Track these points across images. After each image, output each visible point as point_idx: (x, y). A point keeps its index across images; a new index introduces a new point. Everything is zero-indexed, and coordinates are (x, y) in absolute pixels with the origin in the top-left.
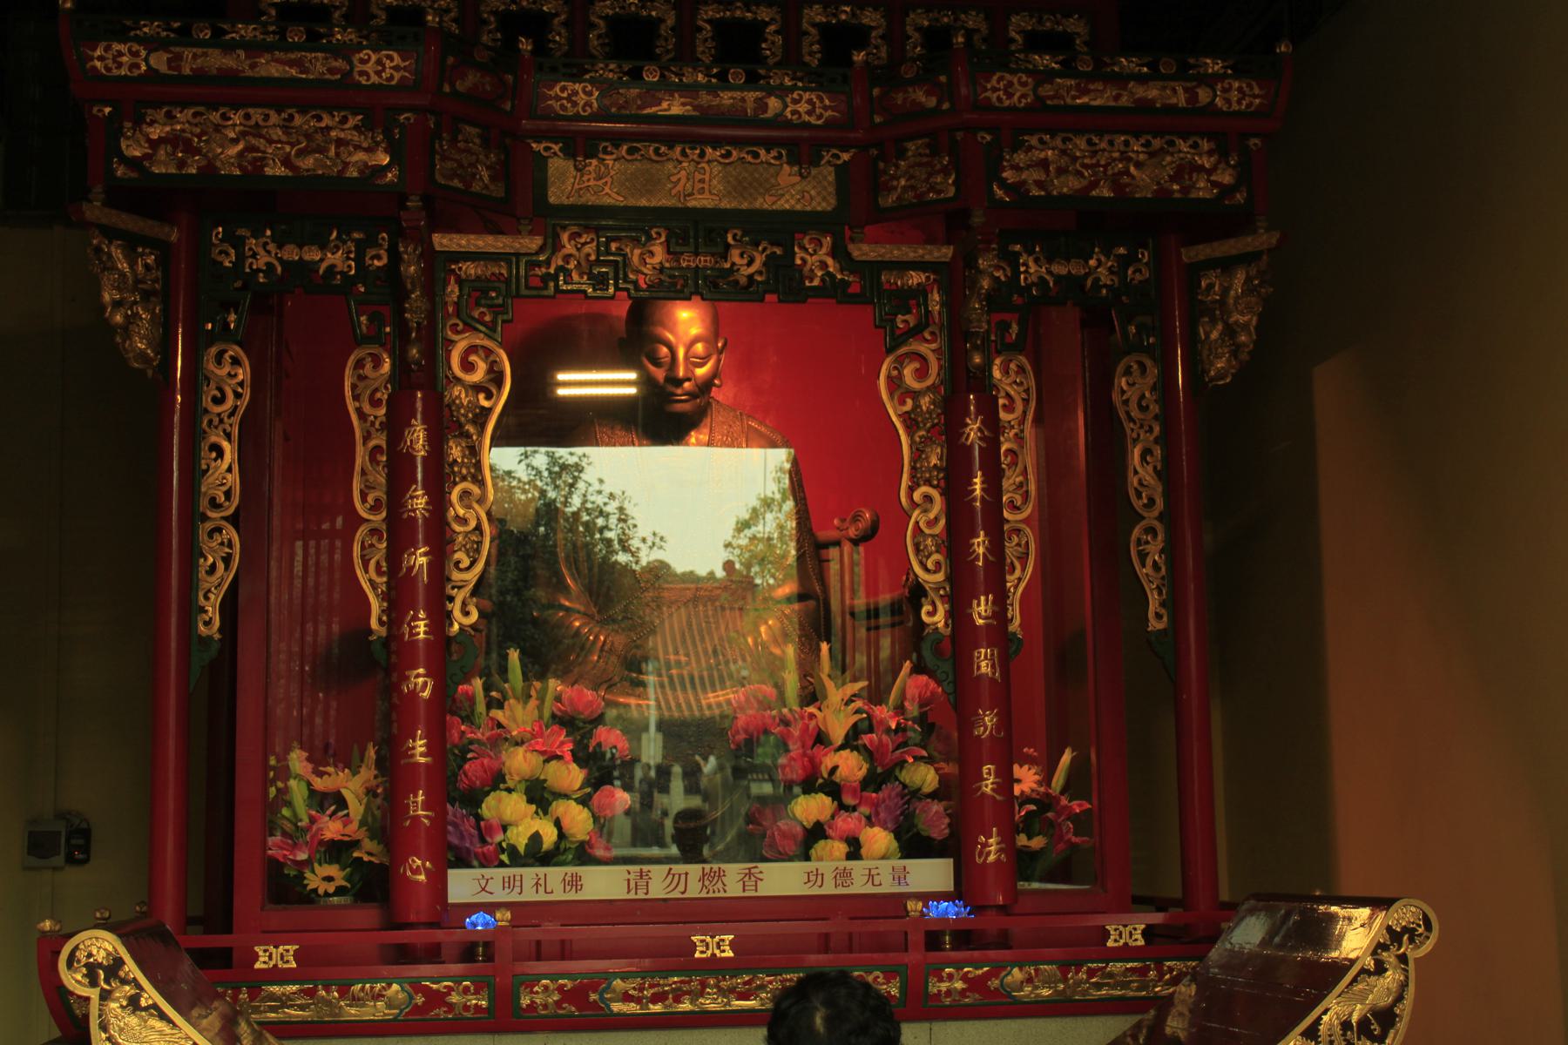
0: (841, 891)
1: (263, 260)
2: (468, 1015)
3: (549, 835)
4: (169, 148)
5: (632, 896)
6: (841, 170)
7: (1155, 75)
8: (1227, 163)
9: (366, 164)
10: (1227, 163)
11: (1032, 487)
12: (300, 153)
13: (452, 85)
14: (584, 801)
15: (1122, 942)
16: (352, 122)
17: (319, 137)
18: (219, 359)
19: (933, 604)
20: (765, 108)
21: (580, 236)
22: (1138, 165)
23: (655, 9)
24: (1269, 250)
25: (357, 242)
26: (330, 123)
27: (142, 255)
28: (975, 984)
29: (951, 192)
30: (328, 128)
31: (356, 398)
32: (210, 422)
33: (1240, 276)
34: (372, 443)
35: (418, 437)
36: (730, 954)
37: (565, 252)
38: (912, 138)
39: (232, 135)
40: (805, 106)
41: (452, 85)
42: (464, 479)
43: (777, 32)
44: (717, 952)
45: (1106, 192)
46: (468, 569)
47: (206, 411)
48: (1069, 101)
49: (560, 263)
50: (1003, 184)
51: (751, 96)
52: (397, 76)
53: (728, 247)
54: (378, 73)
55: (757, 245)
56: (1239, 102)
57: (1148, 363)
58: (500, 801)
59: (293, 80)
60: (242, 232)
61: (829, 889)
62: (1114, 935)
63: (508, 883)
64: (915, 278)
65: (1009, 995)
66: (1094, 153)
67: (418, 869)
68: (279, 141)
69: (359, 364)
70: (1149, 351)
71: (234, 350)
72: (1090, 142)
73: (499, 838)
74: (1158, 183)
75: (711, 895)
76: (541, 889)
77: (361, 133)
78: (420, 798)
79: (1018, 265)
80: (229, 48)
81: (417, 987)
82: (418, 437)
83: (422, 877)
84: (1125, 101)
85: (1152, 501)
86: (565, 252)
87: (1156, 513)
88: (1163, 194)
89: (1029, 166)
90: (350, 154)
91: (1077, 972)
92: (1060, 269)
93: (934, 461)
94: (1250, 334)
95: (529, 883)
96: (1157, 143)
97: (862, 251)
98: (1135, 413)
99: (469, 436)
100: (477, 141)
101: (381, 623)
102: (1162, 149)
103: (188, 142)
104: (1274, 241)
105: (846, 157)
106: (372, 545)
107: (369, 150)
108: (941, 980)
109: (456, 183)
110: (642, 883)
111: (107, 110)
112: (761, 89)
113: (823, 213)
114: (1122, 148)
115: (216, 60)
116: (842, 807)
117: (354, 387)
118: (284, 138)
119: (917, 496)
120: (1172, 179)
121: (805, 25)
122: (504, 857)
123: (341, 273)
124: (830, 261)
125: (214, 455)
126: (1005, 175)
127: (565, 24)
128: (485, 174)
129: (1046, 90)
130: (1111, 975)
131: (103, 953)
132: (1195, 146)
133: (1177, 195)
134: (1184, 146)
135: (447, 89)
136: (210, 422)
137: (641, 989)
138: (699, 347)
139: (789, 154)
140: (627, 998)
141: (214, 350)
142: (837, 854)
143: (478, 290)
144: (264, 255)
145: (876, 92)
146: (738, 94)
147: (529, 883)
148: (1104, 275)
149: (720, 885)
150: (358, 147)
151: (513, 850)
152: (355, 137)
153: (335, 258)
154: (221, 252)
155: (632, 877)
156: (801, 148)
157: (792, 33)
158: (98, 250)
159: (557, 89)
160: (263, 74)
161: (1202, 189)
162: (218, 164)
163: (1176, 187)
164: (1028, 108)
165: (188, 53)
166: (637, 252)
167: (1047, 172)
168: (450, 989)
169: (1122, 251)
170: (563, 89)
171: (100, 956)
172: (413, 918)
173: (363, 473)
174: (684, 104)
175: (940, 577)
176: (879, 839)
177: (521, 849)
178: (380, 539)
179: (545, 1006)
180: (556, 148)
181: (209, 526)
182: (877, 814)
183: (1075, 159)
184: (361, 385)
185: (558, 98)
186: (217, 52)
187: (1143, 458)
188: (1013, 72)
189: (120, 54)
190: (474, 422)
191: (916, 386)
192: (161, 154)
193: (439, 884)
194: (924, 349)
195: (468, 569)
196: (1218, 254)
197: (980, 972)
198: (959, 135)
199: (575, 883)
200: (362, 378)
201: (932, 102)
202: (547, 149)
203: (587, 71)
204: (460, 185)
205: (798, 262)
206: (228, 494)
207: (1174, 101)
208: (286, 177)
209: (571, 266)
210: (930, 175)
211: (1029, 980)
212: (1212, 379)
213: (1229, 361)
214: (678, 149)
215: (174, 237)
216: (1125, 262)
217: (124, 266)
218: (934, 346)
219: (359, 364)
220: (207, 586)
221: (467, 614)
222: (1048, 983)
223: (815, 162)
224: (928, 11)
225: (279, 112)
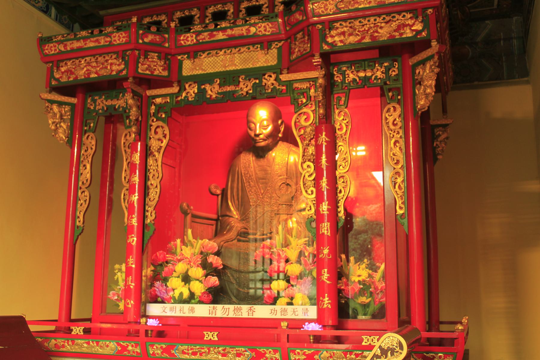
2: (135, 355)
3: (186, 294)
4: (66, 73)
5: (210, 316)
6: (278, 49)
15: (369, 343)
16: (114, 57)
20: (249, 31)
24: (437, 53)
31: (124, 147)
33: (428, 66)
36: (216, 339)
41: (143, 40)
43: (267, 7)
44: (212, 338)
48: (350, 8)
51: (244, 28)
52: (124, 40)
53: (239, 82)
54: (119, 40)
57: (397, 106)
59: (97, 46)
60: (96, 98)
62: (365, 340)
63: (171, 309)
64: (305, 86)
69: (126, 135)
70: (399, 102)
71: (92, 135)
72: (360, 22)
74: (390, 33)
75: (237, 316)
76: (182, 312)
79: (345, 75)
80: (78, 40)
81: (119, 344)
83: (130, 306)
87: (400, 166)
88: (392, 37)
91: (351, 355)
94: (432, 88)
95: (178, 309)
96: (388, 18)
97: (285, 77)
102: (390, 20)
103: (71, 71)
109: (148, 72)
110: (214, 311)
112: (248, 25)
114: (374, 22)
115: (76, 45)
119: (305, 166)
120: (395, 31)
126: (328, 40)
127: (199, 18)
133: (397, 37)
137: (188, 350)
138: (265, 123)
142: (283, 303)
143: (160, 108)
147: (178, 309)
148: (379, 74)
149: (240, 313)
153: (379, 74)
155: (211, 309)
156: (264, 43)
160: (89, 46)
161: (408, 33)
165: (68, 43)
169: (386, 64)
173: (126, 171)
174: (223, 35)
186: (75, 42)
187: (395, 144)
189: (52, 47)
197: (310, 352)
199: (192, 310)
202: (182, 58)
204: (150, 73)
206: (87, 180)
208: (96, 77)
212: (420, 110)
213: (425, 101)
216: (388, 69)
219: (126, 135)
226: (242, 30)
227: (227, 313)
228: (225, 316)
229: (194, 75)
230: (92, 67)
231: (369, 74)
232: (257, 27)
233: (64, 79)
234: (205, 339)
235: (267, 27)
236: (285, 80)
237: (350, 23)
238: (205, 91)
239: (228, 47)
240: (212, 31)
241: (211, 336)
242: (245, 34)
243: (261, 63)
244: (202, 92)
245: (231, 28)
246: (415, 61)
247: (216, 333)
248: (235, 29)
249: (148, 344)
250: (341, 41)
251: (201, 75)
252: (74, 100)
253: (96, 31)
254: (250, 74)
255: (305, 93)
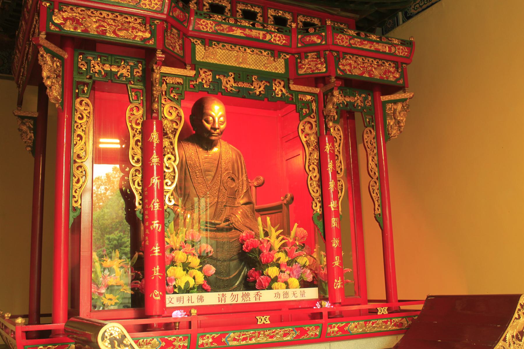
0: (285, 299)
1: (97, 68)
5: (220, 303)
6: (286, 60)
7: (381, 41)
8: (398, 71)
9: (142, 37)
10: (398, 71)
11: (343, 167)
12: (119, 30)
13: (172, 14)
14: (201, 269)
16: (139, 21)
17: (126, 25)
18: (81, 103)
19: (316, 203)
21: (206, 72)
22: (375, 68)
23: (224, 3)
24: (410, 98)
25: (131, 66)
26: (130, 21)
27: (55, 61)
28: (341, 329)
29: (324, 70)
30: (130, 22)
32: (77, 126)
34: (136, 139)
35: (155, 136)
36: (269, 322)
37: (202, 77)
38: (310, 52)
39: (94, 20)
40: (278, 39)
41: (172, 14)
42: (168, 153)
45: (366, 75)
46: (170, 185)
47: (76, 122)
48: (358, 46)
49: (200, 81)
50: (340, 69)
51: (262, 33)
52: (156, 7)
54: (149, 5)
55: (262, 81)
56: (402, 53)
58: (174, 270)
61: (282, 299)
62: (386, 310)
63: (178, 300)
65: (349, 333)
66: (364, 63)
67: (156, 296)
68: (112, 25)
69: (132, 110)
73: (174, 283)
75: (245, 302)
76: (190, 301)
77: (141, 25)
78: (158, 269)
81: (163, 340)
82: (155, 136)
84: (372, 48)
85: (375, 173)
86: (202, 77)
89: (346, 65)
90: (137, 32)
92: (348, 99)
93: (315, 157)
95: (186, 299)
96: (380, 62)
98: (370, 146)
99: (170, 138)
100: (177, 35)
101: (140, 204)
104: (411, 95)
105: (288, 57)
106: (136, 175)
107: (143, 32)
108: (331, 328)
110: (223, 298)
111: (48, 4)
113: (281, 74)
116: (281, 271)
117: (129, 117)
118: (114, 24)
121: (269, 16)
122: (176, 290)
123: (125, 76)
124: (283, 89)
125: (79, 138)
128: (178, 47)
129: (352, 42)
130: (378, 324)
131: (117, 334)
132: (390, 65)
134: (387, 64)
135: (171, 14)
136: (77, 126)
137: (239, 336)
139: (272, 53)
140: (235, 339)
141: (79, 100)
143: (172, 88)
144: (98, 67)
145: (299, 36)
146: (258, 32)
147: (186, 299)
149: (248, 299)
150: (140, 30)
151: (180, 288)
152: (138, 26)
153: (124, 71)
154: (82, 64)
156: (275, 51)
157: (265, 16)
158: (42, 56)
159: (202, 21)
161: (391, 78)
162: (89, 30)
163: (385, 76)
164: (347, 46)
166: (225, 80)
167: (351, 67)
168: (175, 339)
170: (204, 22)
171: (116, 335)
172: (154, 314)
174: (241, 33)
175: (318, 194)
176: (294, 282)
177: (183, 287)
178: (139, 173)
179: (207, 344)
180: (199, 42)
181: (77, 165)
182: (293, 273)
183: (358, 64)
184: (132, 117)
185: (202, 25)
188: (344, 35)
190: (172, 133)
191: (309, 132)
192: (68, 23)
193: (163, 299)
194: (312, 121)
195: (170, 185)
196: (393, 99)
198: (327, 52)
199: (201, 299)
200: (132, 114)
201: (319, 41)
203: (211, 17)
205: (274, 89)
207: (384, 50)
209: (204, 82)
210: (316, 64)
211: (356, 327)
214: (238, 47)
215: (66, 57)
217: (50, 63)
218: (314, 120)
219: (132, 110)
220: (76, 188)
221: (170, 201)
222: (361, 328)
223: (279, 57)
224: (304, 17)
225: (112, 14)
226: (259, 34)
227: (236, 299)
228: (234, 302)
229: (209, 63)
230: (108, 24)
231: (114, 69)
232: (273, 35)
233: (69, 28)
234: (259, 323)
235: (282, 38)
236: (294, 89)
237: (81, 11)
238: (219, 82)
239: (243, 45)
240: (232, 26)
241: (264, 320)
242: (261, 38)
243: (271, 68)
244: (269, 89)
245: (250, 29)
246: (387, 100)
247: (268, 317)
248: (253, 31)
249: (199, 335)
250: (350, 71)
251: (216, 64)
252: (317, 90)
253: (363, 34)
254: (263, 76)
255: (307, 104)
